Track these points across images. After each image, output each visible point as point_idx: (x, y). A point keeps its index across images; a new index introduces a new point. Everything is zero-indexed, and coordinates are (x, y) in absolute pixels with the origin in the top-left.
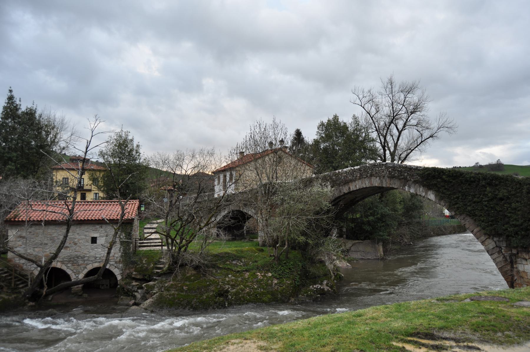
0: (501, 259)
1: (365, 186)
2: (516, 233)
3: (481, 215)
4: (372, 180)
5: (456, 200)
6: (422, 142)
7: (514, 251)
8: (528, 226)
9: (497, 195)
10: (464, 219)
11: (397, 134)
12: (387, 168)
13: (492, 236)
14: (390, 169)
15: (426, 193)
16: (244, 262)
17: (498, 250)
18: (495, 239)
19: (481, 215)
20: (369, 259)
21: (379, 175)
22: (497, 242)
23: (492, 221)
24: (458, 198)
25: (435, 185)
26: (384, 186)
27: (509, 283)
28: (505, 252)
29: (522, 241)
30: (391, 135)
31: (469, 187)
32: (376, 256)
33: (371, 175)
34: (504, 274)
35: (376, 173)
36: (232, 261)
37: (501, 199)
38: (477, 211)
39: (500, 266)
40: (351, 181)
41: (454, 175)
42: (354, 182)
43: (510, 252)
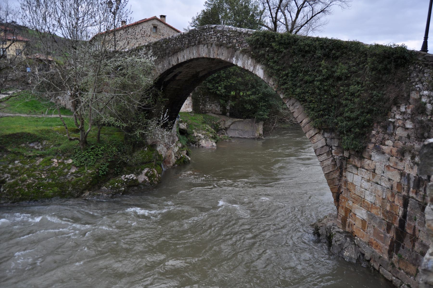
0: (329, 162)
1: (192, 58)
2: (349, 130)
3: (311, 101)
4: (200, 48)
5: (284, 77)
6: (312, 17)
7: (346, 154)
8: (364, 121)
9: (334, 72)
10: (293, 105)
11: (296, 10)
12: (215, 33)
13: (322, 131)
14: (219, 34)
15: (254, 67)
16: (45, 145)
17: (327, 149)
18: (326, 135)
19: (311, 101)
20: (245, 138)
21: (208, 42)
22: (328, 139)
23: (324, 110)
24: (287, 75)
25: (263, 55)
26: (212, 57)
27: (335, 194)
28: (335, 153)
29: (354, 142)
30: (288, 11)
31: (302, 60)
32: (252, 135)
33: (200, 43)
34: (331, 182)
35: (205, 39)
36: (30, 143)
37: (339, 79)
38: (307, 94)
39: (327, 172)
40: (181, 50)
41: (287, 41)
42: (182, 51)
43: (341, 155)
